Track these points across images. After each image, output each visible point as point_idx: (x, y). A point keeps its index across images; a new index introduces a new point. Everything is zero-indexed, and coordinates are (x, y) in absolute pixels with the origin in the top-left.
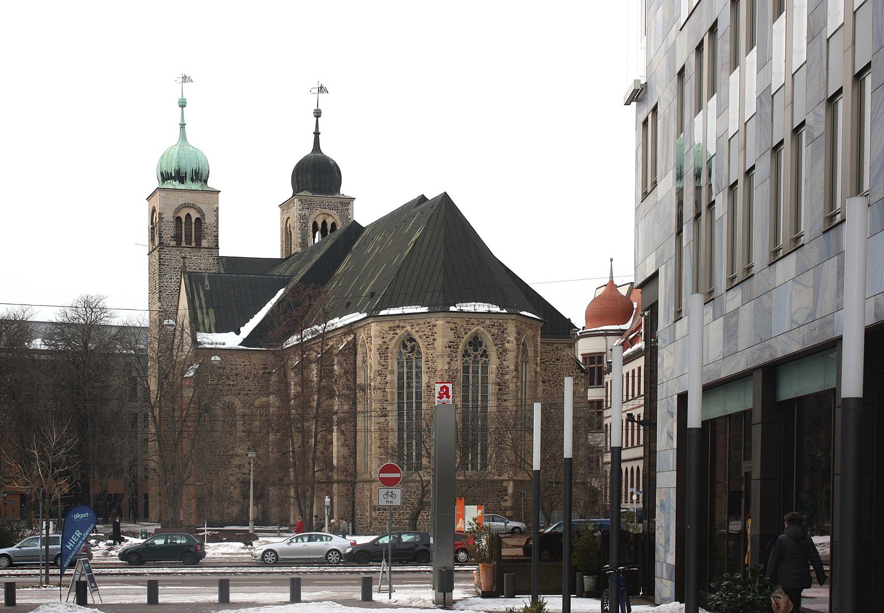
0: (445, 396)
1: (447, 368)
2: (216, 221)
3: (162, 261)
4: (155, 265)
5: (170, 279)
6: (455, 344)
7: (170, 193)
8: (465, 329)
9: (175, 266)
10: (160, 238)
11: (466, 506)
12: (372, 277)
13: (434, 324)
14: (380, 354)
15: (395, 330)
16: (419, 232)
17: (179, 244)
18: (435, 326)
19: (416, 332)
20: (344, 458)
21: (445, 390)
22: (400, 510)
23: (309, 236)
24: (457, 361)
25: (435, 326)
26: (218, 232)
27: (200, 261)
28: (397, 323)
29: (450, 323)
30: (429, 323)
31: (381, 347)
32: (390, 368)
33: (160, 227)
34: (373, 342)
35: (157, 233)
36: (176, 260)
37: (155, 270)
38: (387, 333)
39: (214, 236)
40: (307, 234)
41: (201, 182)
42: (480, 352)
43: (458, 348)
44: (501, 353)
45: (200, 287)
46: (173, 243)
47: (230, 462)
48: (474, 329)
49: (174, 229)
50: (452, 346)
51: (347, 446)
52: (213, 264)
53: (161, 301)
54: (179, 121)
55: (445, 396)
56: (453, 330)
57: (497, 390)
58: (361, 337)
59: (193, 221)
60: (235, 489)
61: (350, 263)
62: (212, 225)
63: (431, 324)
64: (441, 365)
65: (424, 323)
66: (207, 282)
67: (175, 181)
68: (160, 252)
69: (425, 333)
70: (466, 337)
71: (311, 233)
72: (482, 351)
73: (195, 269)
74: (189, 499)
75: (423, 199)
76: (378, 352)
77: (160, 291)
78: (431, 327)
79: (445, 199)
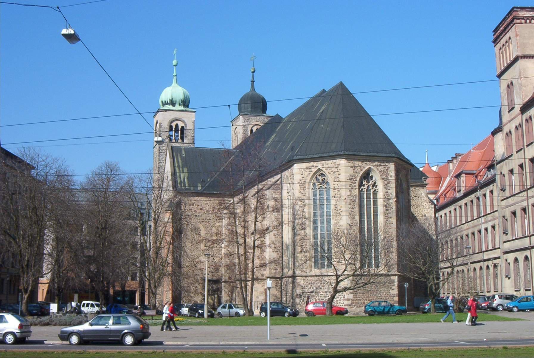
1: (349, 195)
6: (354, 177)
14: (300, 185)
15: (310, 169)
22: (316, 297)
25: (339, 165)
32: (307, 195)
34: (295, 178)
38: (305, 171)
42: (371, 183)
44: (386, 185)
45: (179, 155)
48: (367, 168)
50: (351, 179)
51: (276, 252)
54: (251, 79)
57: (384, 210)
58: (286, 176)
59: (180, 128)
63: (337, 164)
64: (344, 193)
66: (183, 152)
69: (332, 170)
70: (362, 173)
75: (324, 91)
76: (298, 185)
79: (341, 87)
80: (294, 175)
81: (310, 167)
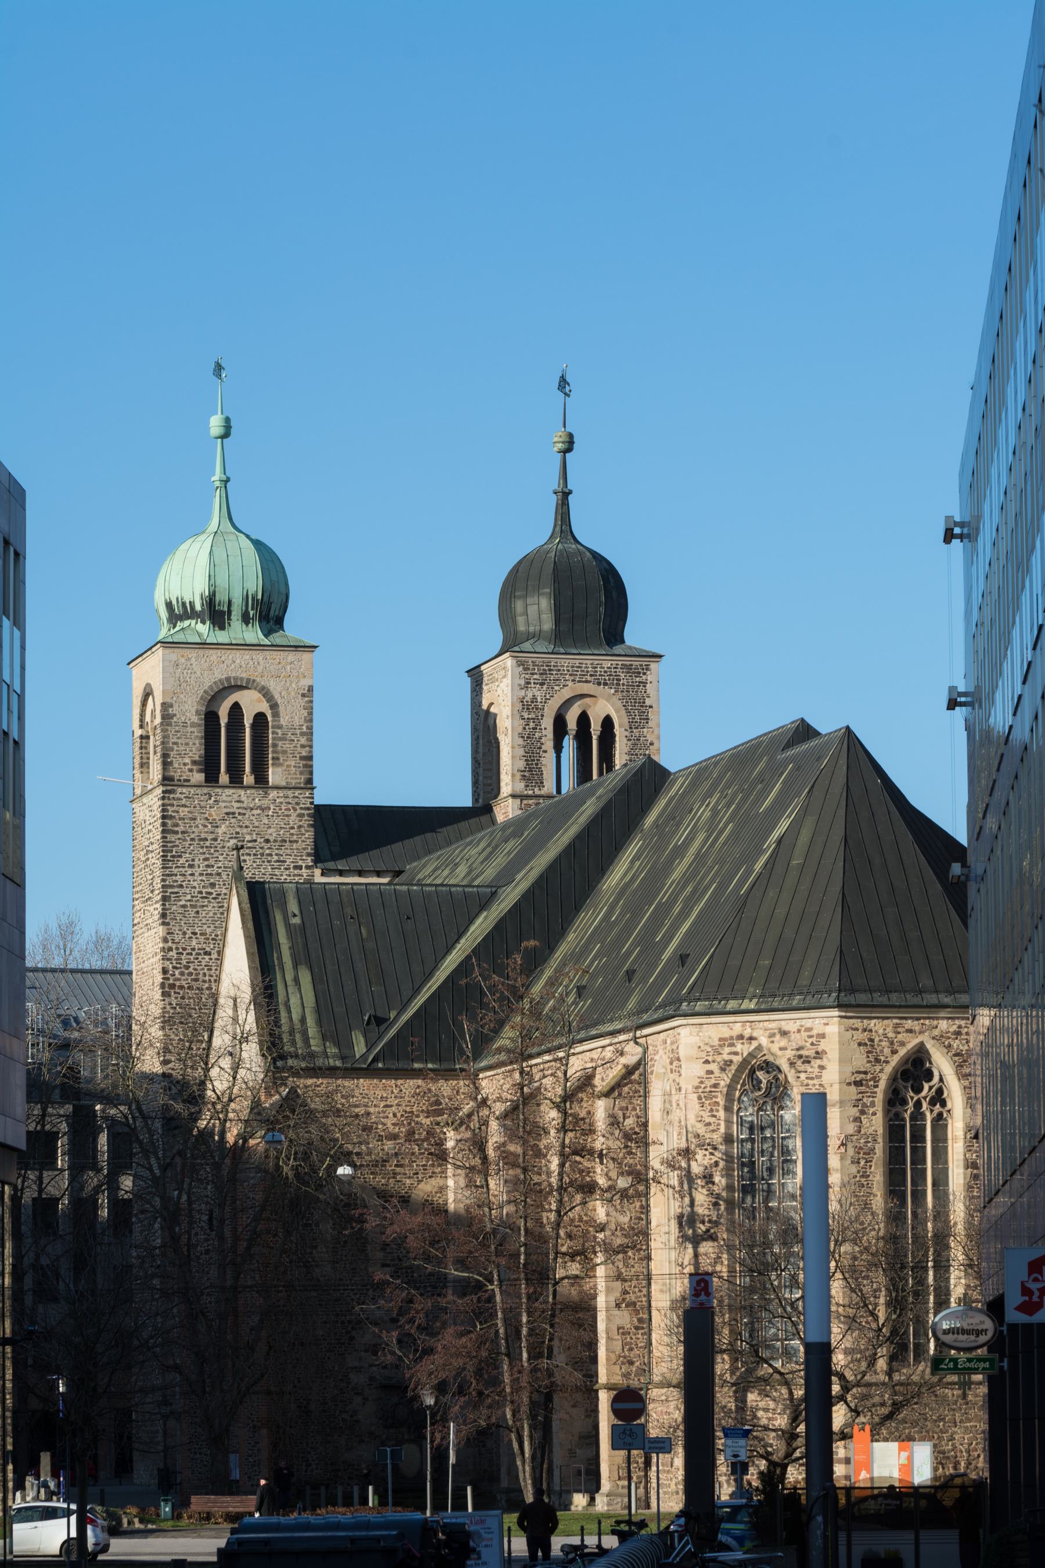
0: (703, 1293)
2: (306, 721)
3: (169, 822)
4: (149, 831)
5: (191, 866)
6: (869, 1076)
7: (186, 652)
8: (892, 1043)
9: (203, 836)
10: (166, 764)
11: (875, 1444)
12: (684, 914)
13: (820, 1032)
14: (700, 1098)
16: (789, 816)
17: (211, 777)
18: (823, 1036)
19: (781, 1049)
20: (623, 1334)
21: (703, 1285)
23: (545, 752)
24: (874, 1114)
25: (823, 1036)
26: (311, 747)
27: (266, 821)
28: (737, 1029)
29: (857, 1029)
30: (809, 1029)
31: (702, 1082)
33: (164, 737)
34: (683, 1071)
35: (155, 753)
36: (207, 819)
37: (152, 844)
39: (302, 758)
40: (540, 748)
41: (268, 622)
43: (877, 1086)
46: (199, 777)
47: (352, 1338)
48: (913, 1043)
49: (200, 744)
52: (300, 827)
53: (168, 924)
54: (554, 483)
55: (703, 1293)
56: (866, 1044)
59: (248, 722)
60: (364, 1404)
61: (637, 864)
62: (298, 732)
63: (814, 1032)
65: (799, 1031)
66: (293, 907)
67: (203, 622)
68: (166, 801)
70: (895, 1060)
71: (549, 744)
72: (934, 1090)
73: (255, 841)
74: (254, 1426)
75: (803, 732)
76: (696, 1095)
77: (165, 899)
78: (814, 1040)
80: (683, 1063)
81: (731, 1038)
